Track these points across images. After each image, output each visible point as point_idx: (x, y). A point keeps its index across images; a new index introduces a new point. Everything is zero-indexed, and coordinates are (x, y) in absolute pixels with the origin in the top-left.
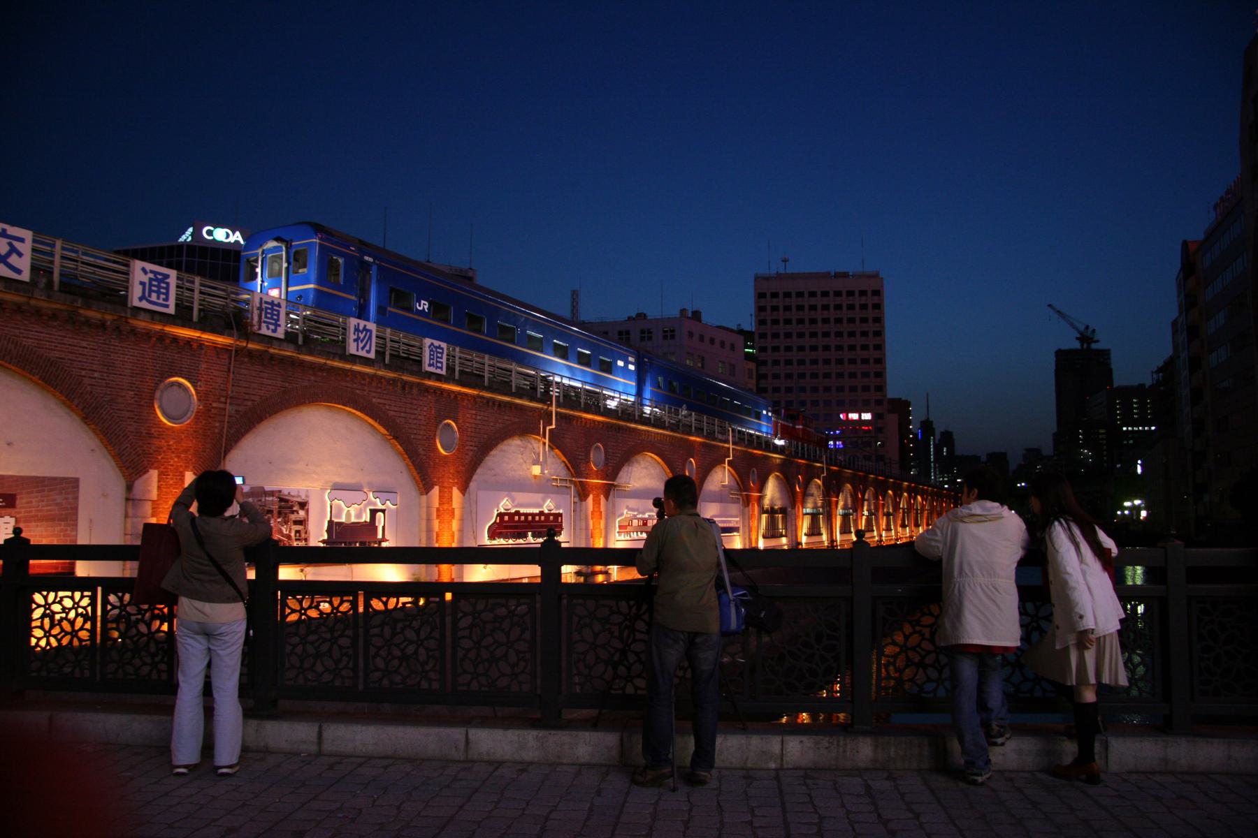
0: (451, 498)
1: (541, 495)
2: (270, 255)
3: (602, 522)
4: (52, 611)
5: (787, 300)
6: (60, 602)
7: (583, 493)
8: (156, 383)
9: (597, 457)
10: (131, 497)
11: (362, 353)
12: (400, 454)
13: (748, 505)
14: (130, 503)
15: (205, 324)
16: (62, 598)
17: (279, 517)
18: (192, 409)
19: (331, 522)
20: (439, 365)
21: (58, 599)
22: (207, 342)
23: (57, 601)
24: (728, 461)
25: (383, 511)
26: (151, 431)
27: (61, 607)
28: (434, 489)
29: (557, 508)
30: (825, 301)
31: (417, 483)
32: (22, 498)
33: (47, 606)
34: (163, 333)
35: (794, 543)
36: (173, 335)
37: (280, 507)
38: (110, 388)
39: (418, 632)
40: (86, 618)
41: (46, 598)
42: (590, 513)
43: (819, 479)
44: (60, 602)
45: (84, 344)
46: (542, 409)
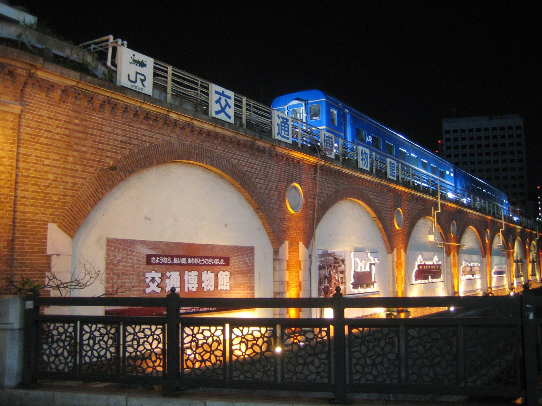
0: (401, 255)
1: (432, 253)
2: (291, 110)
3: (457, 269)
4: (94, 335)
5: (463, 134)
6: (143, 332)
7: (448, 253)
8: (286, 187)
9: (453, 228)
10: (278, 258)
11: (364, 168)
12: (380, 229)
13: (392, 250)
14: (277, 262)
15: (303, 149)
16: (58, 327)
17: (334, 269)
18: (301, 203)
19: (355, 271)
20: (394, 174)
21: (56, 328)
22: (306, 161)
23: (200, 332)
24: (502, 230)
25: (374, 264)
26: (284, 218)
27: (253, 337)
28: (284, 245)
29: (439, 261)
30: (479, 134)
31: (386, 246)
32: (232, 260)
33: (91, 332)
34: (288, 155)
35: (527, 280)
36: (293, 157)
37: (335, 263)
38: (268, 190)
39: (383, 349)
40: (71, 338)
41: (90, 328)
42: (452, 264)
43: (535, 241)
44: (143, 332)
45: (256, 162)
46: (433, 200)
